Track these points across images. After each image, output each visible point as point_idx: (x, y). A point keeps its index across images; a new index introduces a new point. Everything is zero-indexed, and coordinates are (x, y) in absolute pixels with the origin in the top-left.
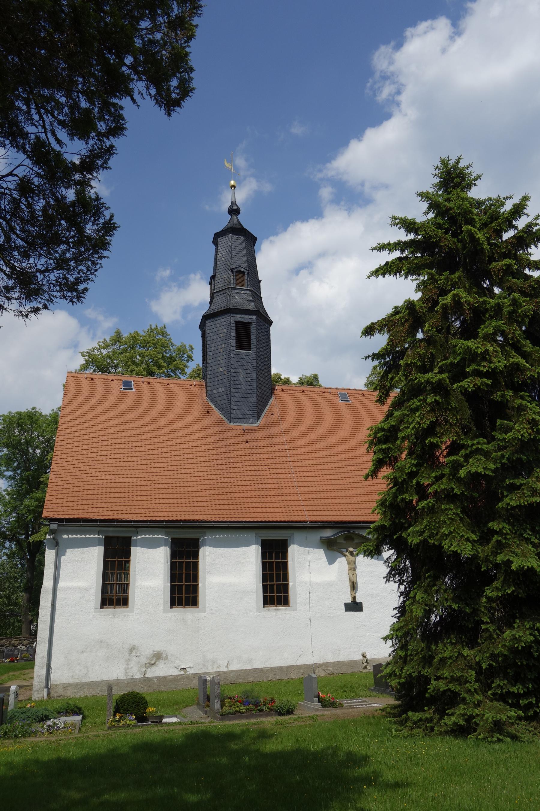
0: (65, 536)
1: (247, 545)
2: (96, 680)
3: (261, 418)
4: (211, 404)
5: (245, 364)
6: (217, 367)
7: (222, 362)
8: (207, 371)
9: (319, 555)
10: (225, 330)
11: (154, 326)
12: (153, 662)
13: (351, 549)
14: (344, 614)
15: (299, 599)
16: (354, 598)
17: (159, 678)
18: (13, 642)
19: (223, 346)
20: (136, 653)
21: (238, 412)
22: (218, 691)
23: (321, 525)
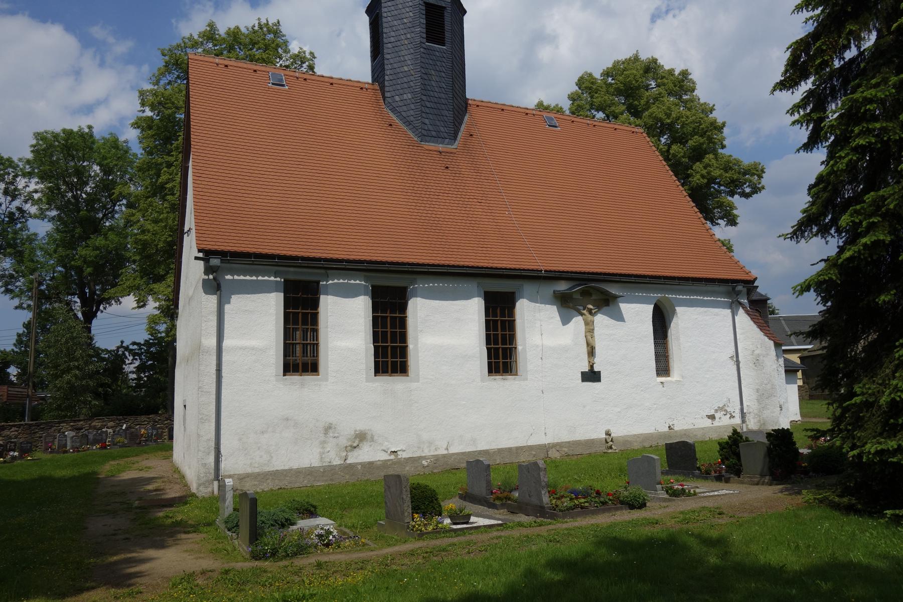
0: (229, 277)
1: (468, 297)
2: (282, 468)
3: (458, 139)
4: (391, 114)
5: (438, 63)
6: (399, 65)
7: (406, 58)
8: (384, 69)
9: (551, 312)
10: (411, 14)
11: (264, 21)
12: (355, 445)
13: (590, 306)
14: (724, 376)
15: (530, 367)
16: (592, 367)
17: (363, 465)
18: (93, 424)
19: (409, 36)
20: (333, 433)
21: (431, 128)
22: (546, 480)
23: (557, 274)
